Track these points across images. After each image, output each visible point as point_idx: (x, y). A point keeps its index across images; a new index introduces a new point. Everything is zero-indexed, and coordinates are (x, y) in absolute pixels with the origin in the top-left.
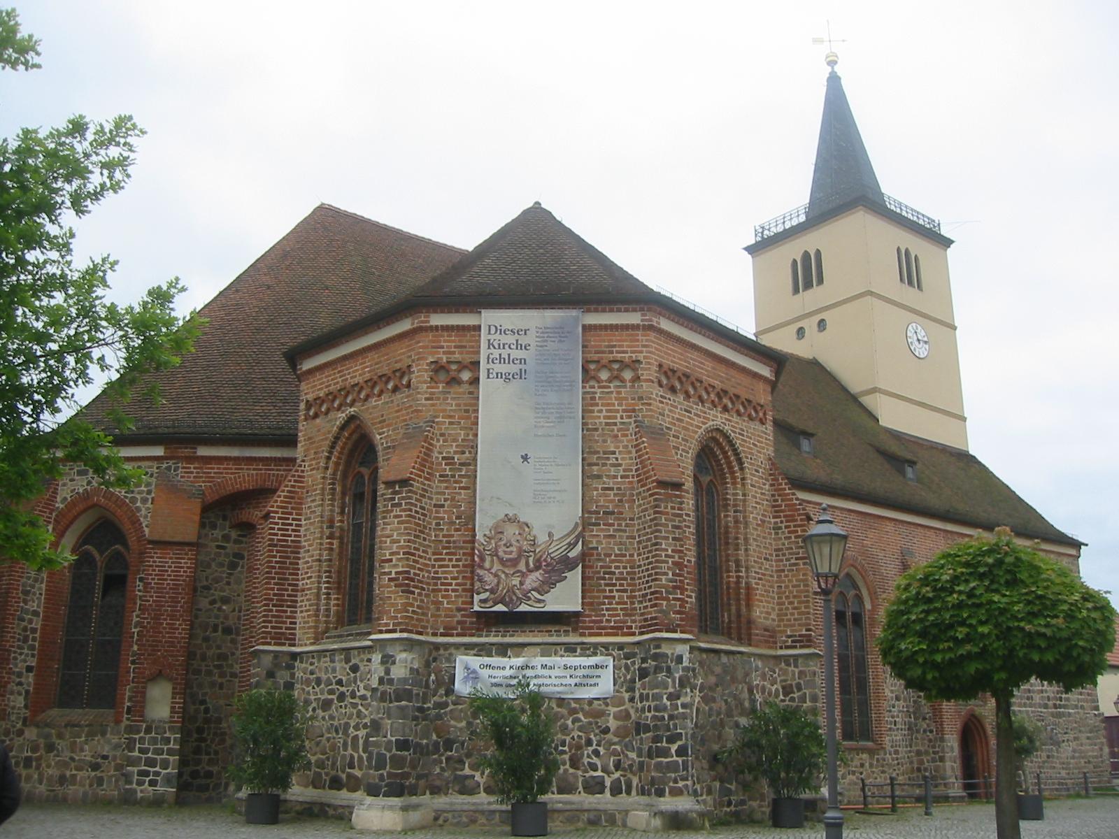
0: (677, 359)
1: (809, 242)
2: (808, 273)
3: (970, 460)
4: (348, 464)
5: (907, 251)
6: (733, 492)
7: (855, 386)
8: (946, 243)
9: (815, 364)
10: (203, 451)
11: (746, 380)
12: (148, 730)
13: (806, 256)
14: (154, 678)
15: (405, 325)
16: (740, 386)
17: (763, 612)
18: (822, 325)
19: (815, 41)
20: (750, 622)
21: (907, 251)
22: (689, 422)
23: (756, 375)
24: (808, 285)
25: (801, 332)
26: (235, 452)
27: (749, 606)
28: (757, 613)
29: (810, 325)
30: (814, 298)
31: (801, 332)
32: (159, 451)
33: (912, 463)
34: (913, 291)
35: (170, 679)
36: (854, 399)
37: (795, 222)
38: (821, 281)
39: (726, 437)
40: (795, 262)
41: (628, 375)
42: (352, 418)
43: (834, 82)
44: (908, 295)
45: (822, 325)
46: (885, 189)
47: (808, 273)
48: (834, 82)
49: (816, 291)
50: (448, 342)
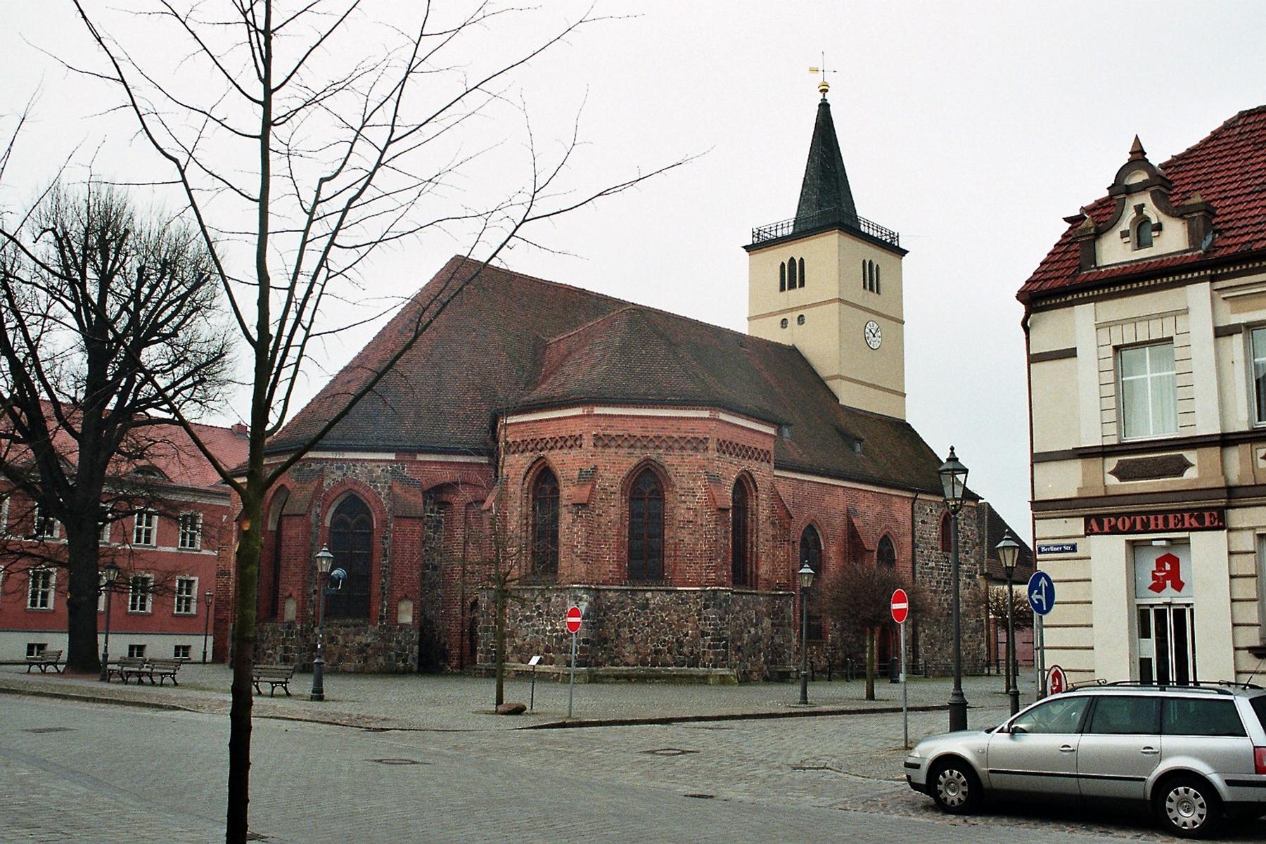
0: (727, 434)
1: (796, 250)
2: (793, 276)
3: (904, 430)
4: (536, 483)
5: (871, 263)
6: (752, 503)
7: (823, 373)
8: (903, 252)
9: (793, 350)
10: (420, 457)
11: (760, 438)
12: (401, 630)
13: (792, 260)
14: (401, 600)
15: (578, 411)
16: (759, 444)
17: (764, 570)
18: (801, 319)
19: (811, 70)
20: (757, 576)
21: (871, 263)
22: (731, 469)
23: (766, 434)
24: (792, 286)
25: (784, 323)
26: (441, 458)
27: (757, 568)
28: (761, 571)
29: (792, 318)
30: (796, 296)
31: (784, 323)
32: (392, 457)
33: (860, 440)
34: (873, 295)
35: (411, 599)
36: (821, 382)
37: (785, 232)
38: (802, 284)
39: (751, 476)
40: (783, 264)
41: (701, 446)
42: (540, 458)
43: (824, 107)
44: (871, 299)
45: (801, 319)
46: (860, 212)
47: (793, 276)
48: (824, 107)
49: (798, 291)
50: (603, 423)
